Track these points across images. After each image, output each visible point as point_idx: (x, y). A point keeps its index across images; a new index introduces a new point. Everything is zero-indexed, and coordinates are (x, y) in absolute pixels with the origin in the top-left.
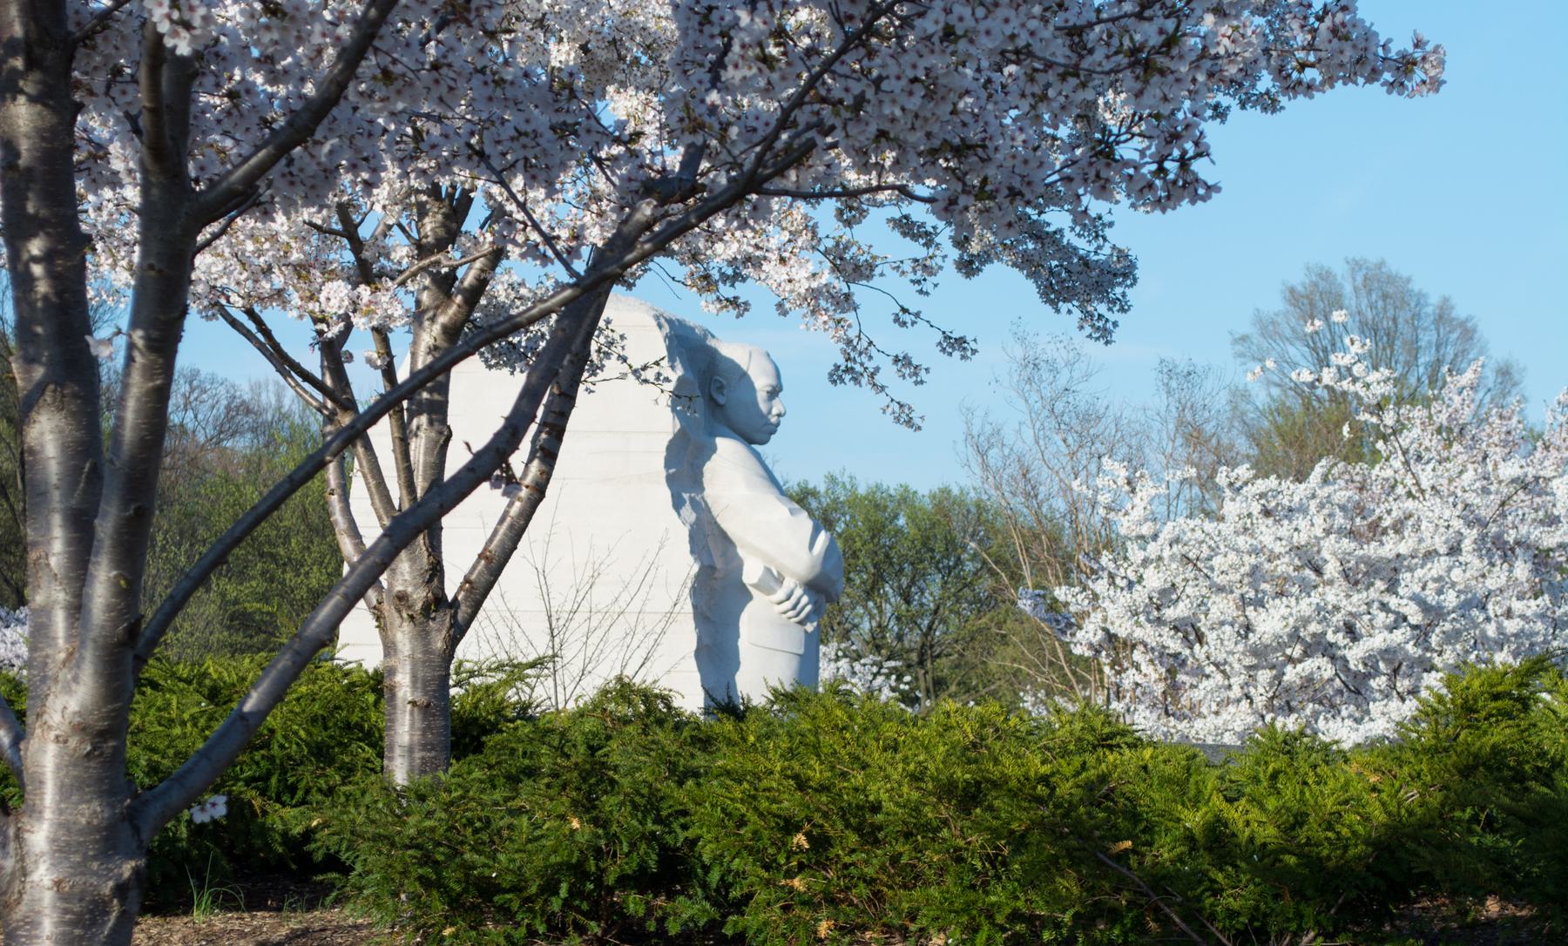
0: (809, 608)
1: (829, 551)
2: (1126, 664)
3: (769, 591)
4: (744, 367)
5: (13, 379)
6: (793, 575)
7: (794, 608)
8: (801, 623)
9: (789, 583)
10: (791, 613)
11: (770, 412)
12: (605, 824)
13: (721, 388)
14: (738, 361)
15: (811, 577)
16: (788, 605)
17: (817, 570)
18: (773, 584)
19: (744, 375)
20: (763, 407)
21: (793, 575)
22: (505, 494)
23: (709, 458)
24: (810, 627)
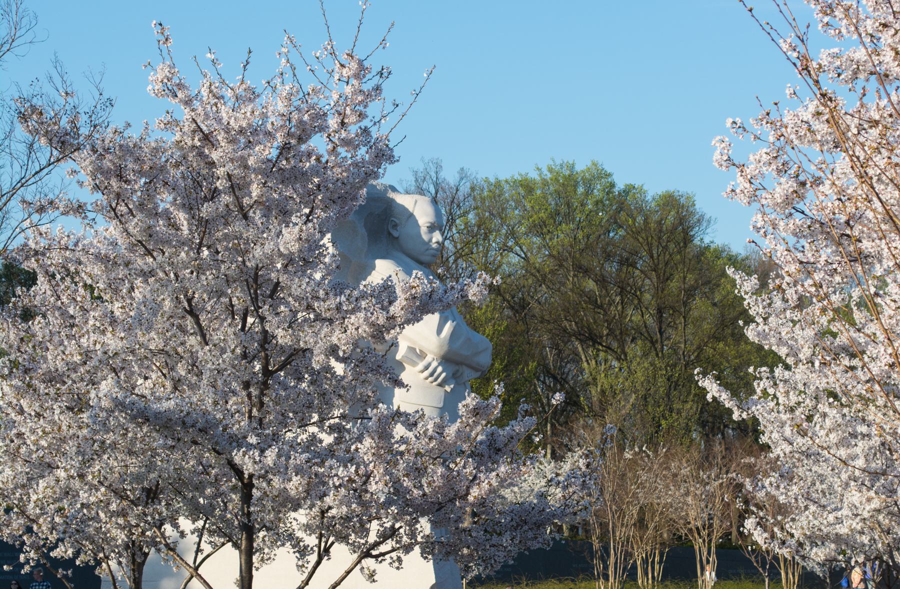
0: (444, 375)
1: (453, 335)
2: (512, 184)
3: (414, 364)
4: (411, 210)
5: (547, 431)
6: (431, 352)
7: (432, 375)
8: (440, 385)
9: (429, 358)
10: (431, 379)
11: (430, 240)
12: (67, 517)
13: (395, 226)
14: (407, 206)
15: (442, 353)
16: (427, 373)
17: (445, 348)
18: (415, 359)
19: (411, 215)
20: (425, 237)
21: (431, 352)
22: (403, 369)
23: (370, 274)
24: (448, 389)
